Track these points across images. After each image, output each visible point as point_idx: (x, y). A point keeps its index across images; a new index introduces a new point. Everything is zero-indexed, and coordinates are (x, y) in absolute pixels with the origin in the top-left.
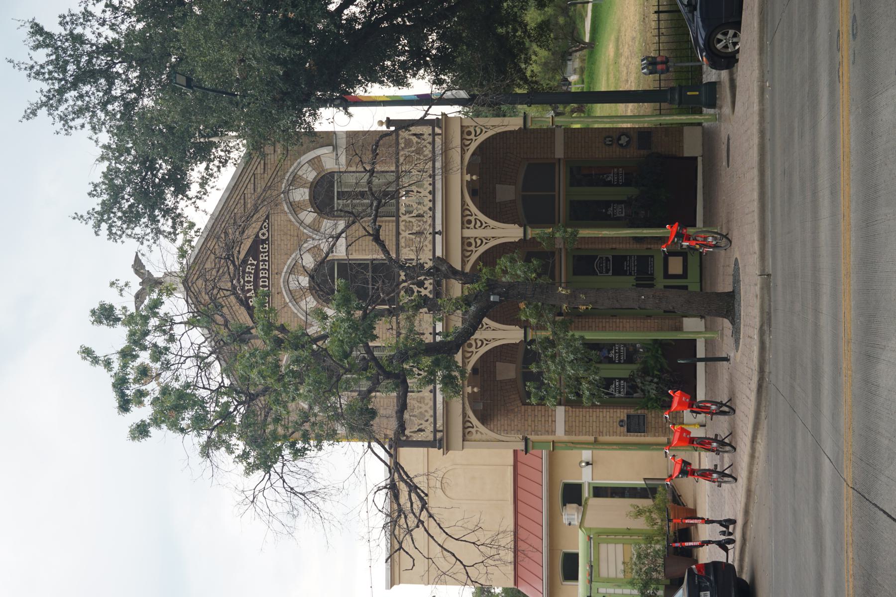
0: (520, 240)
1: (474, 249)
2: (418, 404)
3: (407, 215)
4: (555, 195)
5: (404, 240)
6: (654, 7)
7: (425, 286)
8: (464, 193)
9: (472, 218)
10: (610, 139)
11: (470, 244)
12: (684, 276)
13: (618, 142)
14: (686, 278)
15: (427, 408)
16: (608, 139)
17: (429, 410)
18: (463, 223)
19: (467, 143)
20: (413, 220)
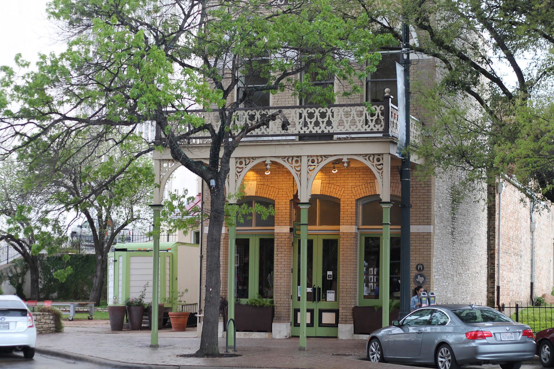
0: (299, 199)
1: (293, 166)
2: (350, 120)
3: (331, 114)
4: (316, 225)
5: (362, 110)
6: (521, 304)
7: (327, 127)
8: (261, 159)
9: (243, 165)
10: (422, 269)
11: (297, 161)
12: (321, 324)
13: (419, 275)
14: (319, 326)
15: (359, 127)
16: (421, 267)
17: (370, 128)
18: (240, 158)
19: (371, 158)
20: (364, 117)
